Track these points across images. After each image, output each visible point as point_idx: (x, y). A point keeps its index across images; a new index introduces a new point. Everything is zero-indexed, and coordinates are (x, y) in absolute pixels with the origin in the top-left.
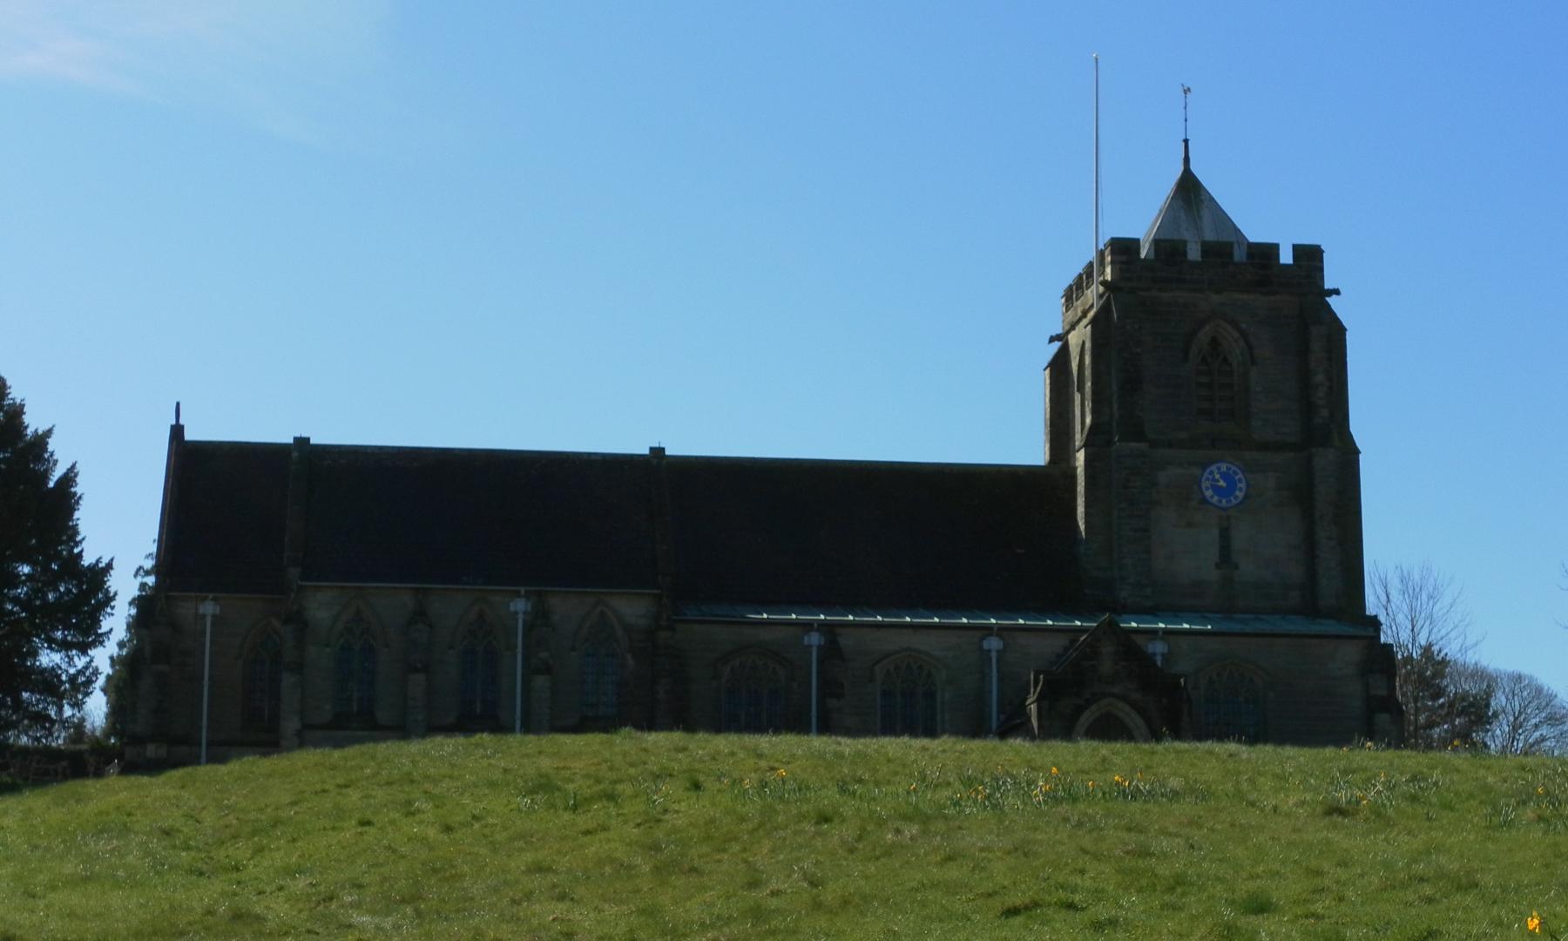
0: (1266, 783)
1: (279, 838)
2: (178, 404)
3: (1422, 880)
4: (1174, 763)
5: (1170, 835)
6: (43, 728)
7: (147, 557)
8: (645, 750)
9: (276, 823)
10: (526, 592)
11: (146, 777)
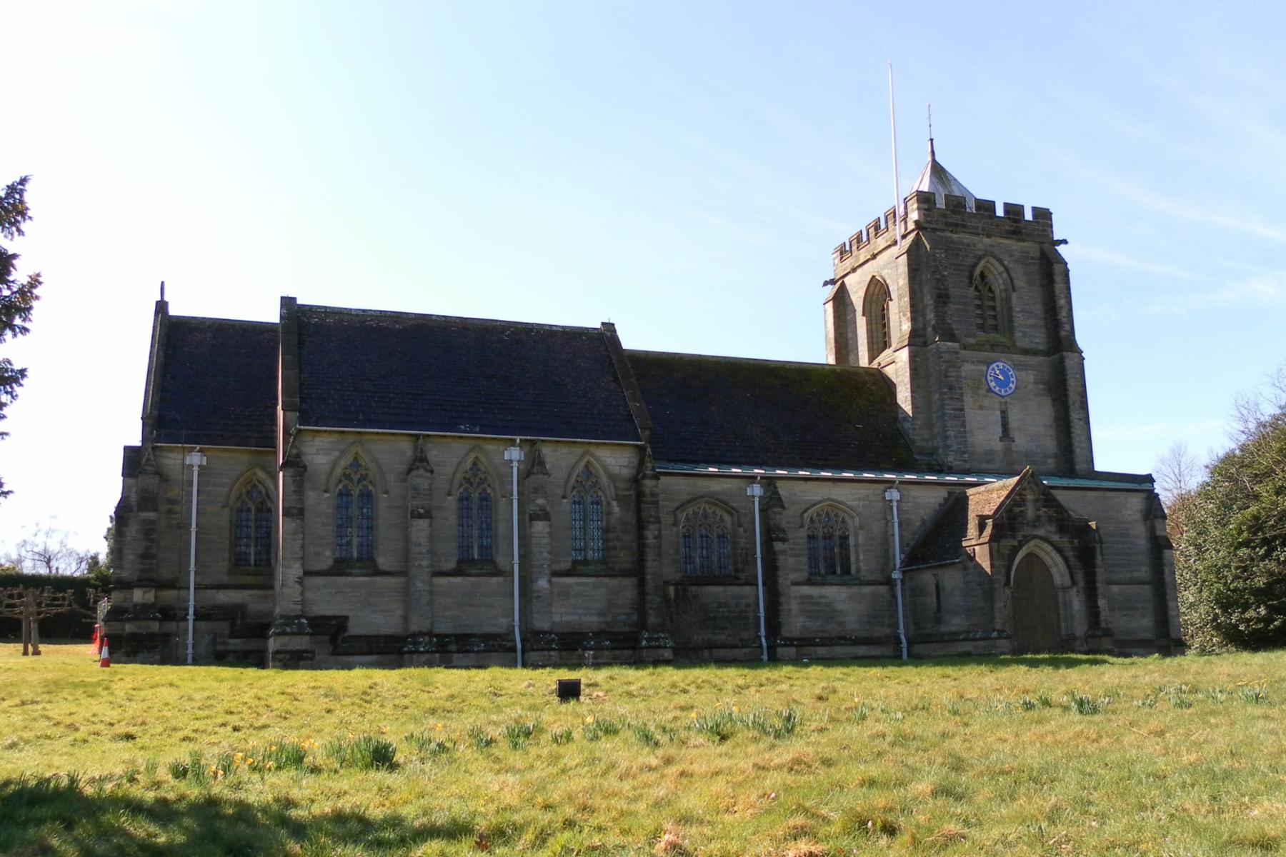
2: (163, 283)
10: (521, 440)
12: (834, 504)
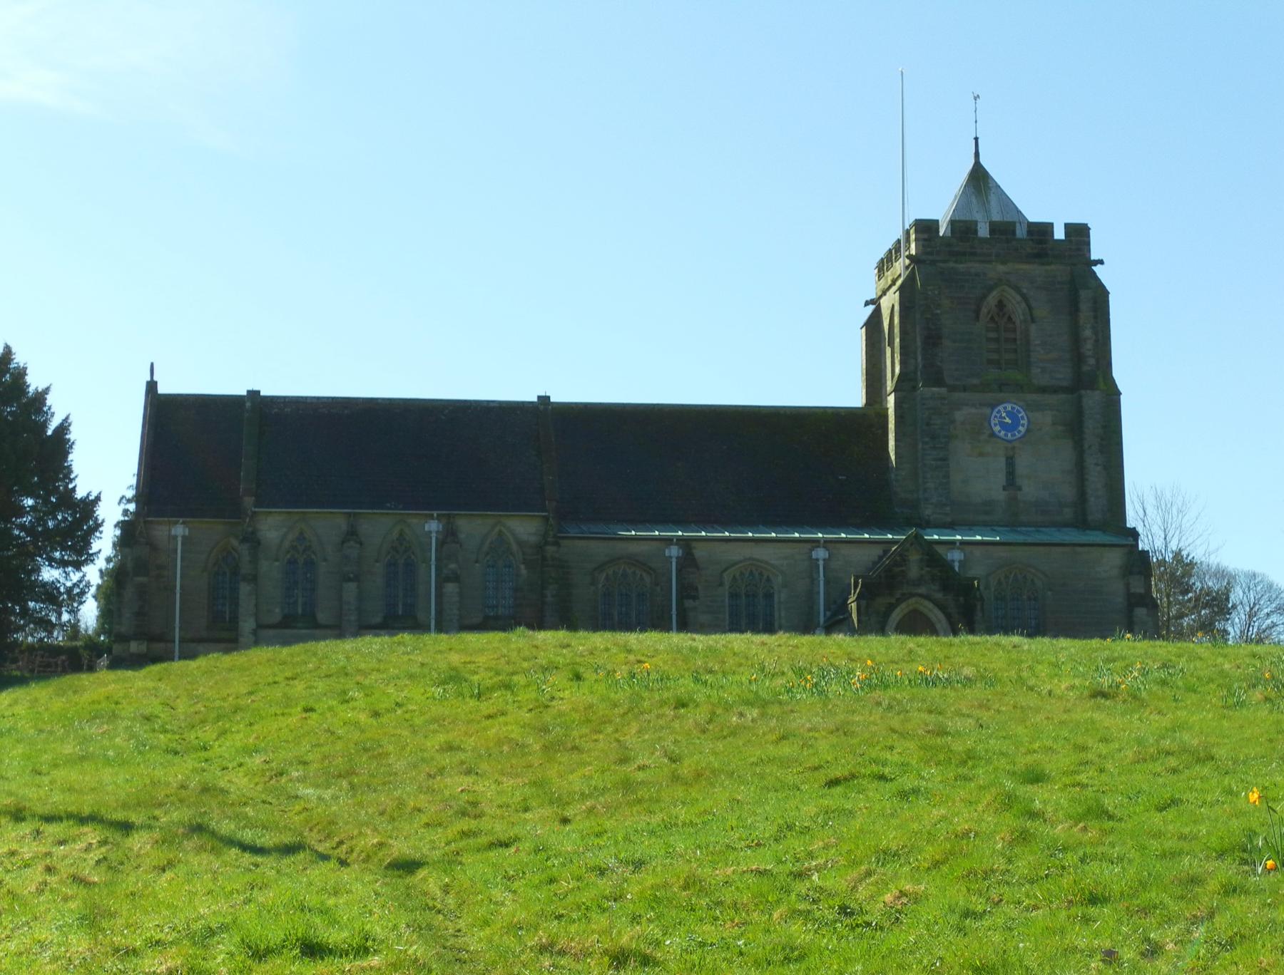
0: (1043, 670)
1: (238, 723)
3: (1168, 753)
4: (968, 654)
5: (964, 716)
6: (45, 630)
7: (129, 488)
8: (536, 647)
9: (236, 710)
10: (438, 515)
11: (130, 672)
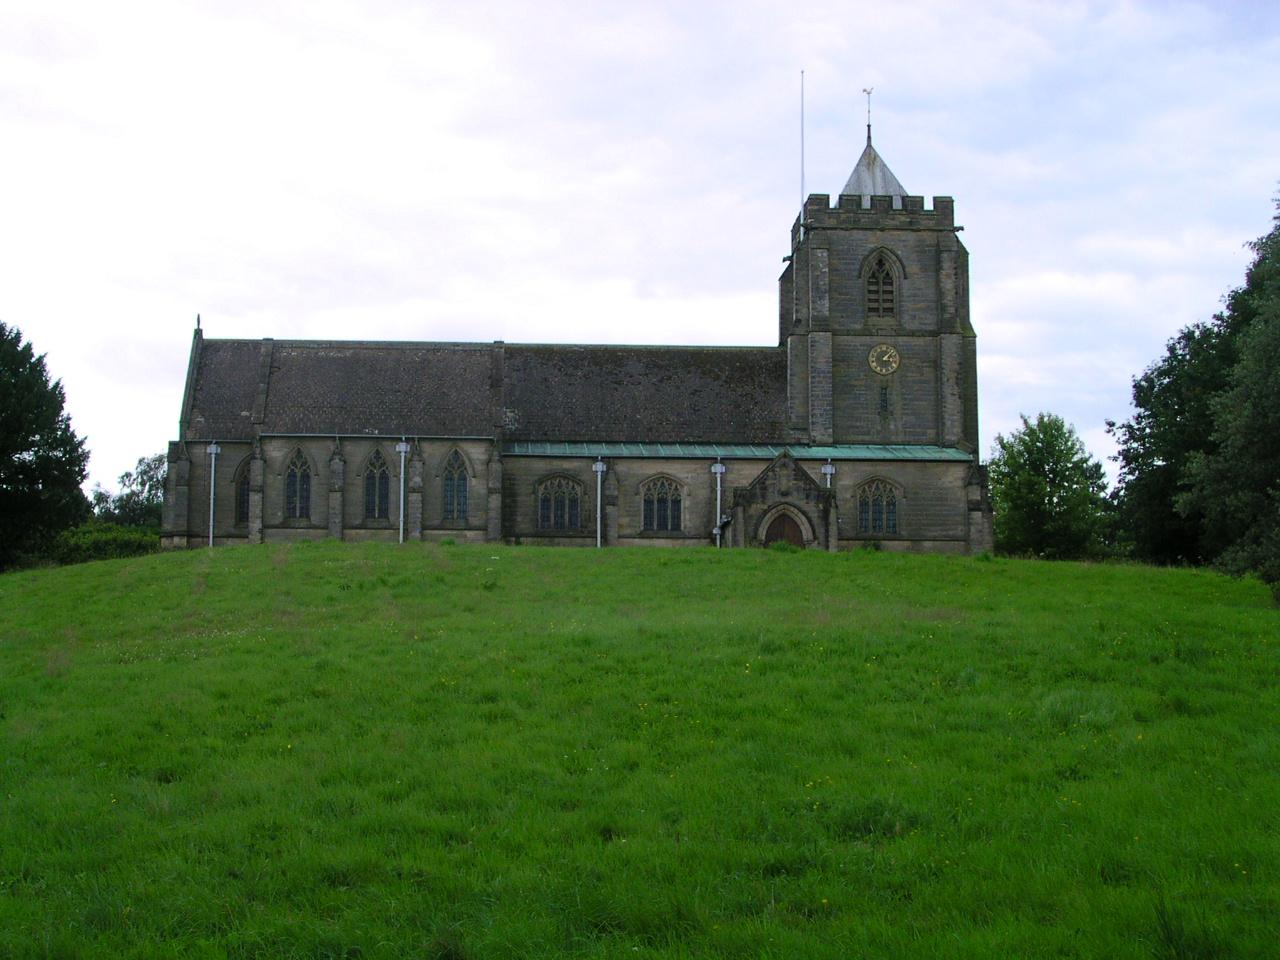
12: (665, 480)
